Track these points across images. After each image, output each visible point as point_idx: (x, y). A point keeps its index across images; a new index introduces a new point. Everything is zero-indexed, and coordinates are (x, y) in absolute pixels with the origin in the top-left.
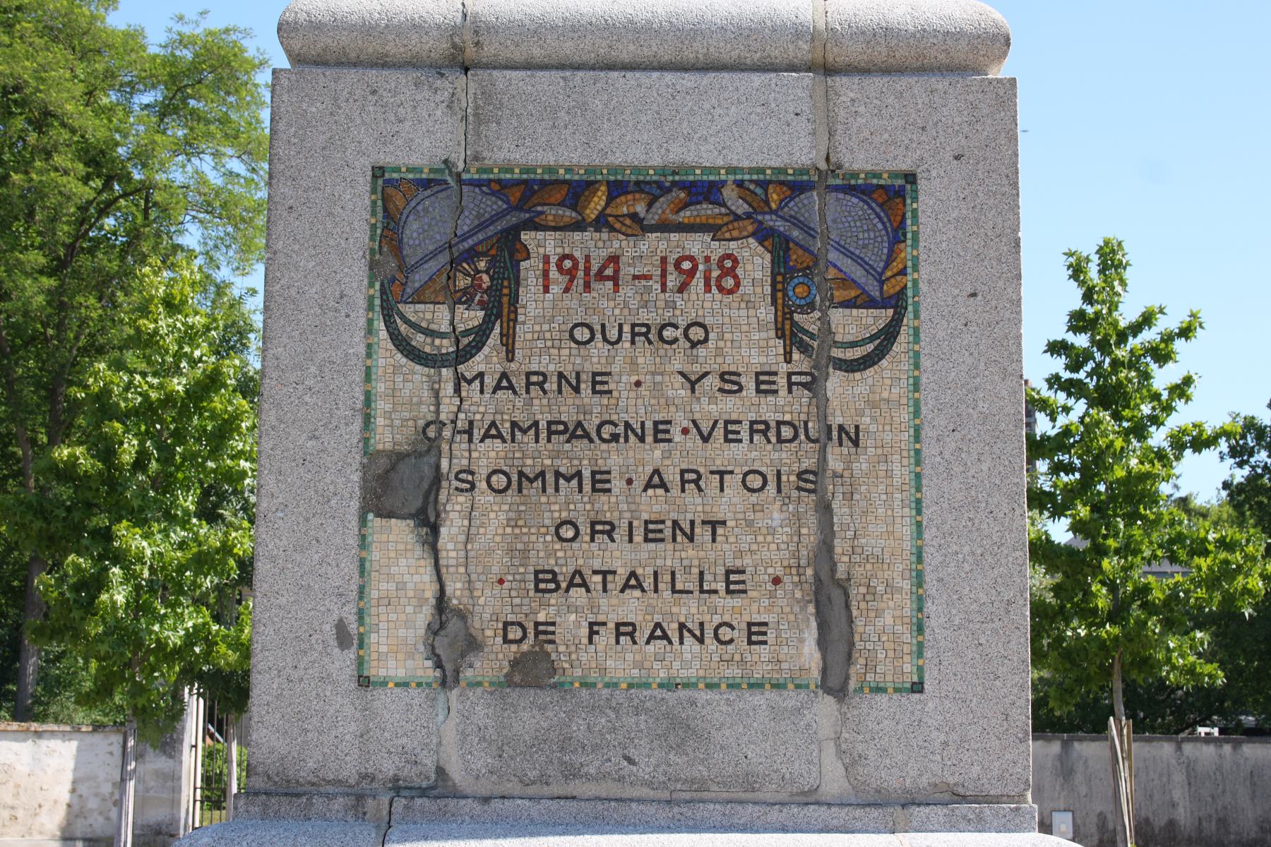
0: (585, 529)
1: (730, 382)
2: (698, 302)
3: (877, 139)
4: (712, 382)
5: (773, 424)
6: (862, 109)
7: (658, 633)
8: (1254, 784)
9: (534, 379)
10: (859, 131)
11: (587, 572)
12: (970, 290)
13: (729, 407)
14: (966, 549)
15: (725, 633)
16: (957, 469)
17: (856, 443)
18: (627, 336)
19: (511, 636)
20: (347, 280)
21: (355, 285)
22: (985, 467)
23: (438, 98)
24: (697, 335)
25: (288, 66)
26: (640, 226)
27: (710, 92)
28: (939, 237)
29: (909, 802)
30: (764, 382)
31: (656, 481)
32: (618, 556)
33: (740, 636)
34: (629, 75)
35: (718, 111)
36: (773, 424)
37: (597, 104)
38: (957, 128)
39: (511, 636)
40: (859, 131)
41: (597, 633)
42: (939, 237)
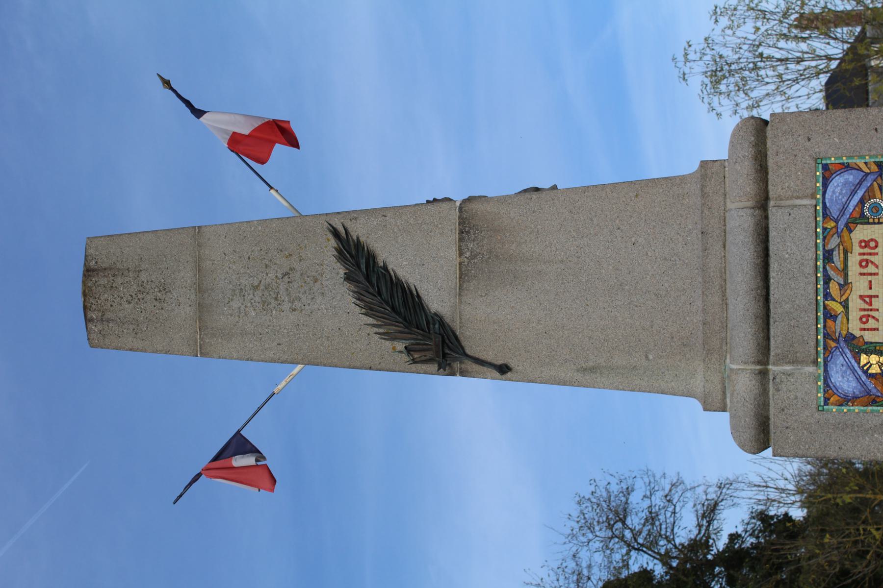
26: (845, 285)
37: (787, 307)
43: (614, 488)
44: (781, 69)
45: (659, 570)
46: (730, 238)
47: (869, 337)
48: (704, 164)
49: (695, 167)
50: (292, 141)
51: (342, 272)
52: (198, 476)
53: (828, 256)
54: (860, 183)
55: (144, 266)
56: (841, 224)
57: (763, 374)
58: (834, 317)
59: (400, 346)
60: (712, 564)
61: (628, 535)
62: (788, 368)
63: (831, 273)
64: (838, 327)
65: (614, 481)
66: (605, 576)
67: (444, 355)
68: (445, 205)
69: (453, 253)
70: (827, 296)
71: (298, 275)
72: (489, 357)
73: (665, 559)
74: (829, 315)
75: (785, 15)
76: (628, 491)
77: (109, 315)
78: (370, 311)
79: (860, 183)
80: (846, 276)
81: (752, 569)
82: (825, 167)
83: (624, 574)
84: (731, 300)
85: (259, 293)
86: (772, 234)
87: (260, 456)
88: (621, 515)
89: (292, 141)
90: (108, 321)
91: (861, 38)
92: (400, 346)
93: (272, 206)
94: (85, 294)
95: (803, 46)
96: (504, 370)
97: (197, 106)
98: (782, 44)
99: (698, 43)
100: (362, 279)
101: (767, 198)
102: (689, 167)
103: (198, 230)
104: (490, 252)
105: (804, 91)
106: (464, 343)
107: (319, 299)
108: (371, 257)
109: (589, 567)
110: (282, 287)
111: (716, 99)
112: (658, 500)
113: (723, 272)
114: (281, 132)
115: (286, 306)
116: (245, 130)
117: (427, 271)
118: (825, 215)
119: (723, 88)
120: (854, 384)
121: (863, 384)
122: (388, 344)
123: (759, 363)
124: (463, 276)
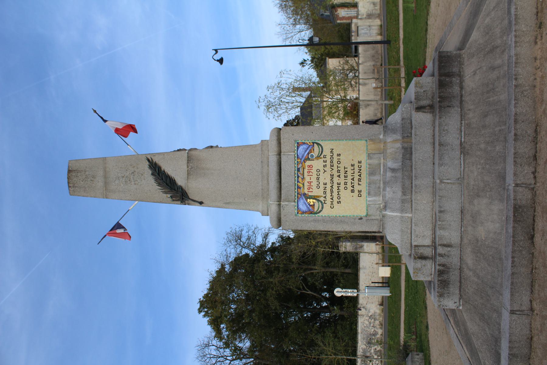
1: (325, 166)
2: (314, 171)
4: (325, 168)
7: (360, 176)
24: (318, 171)
26: (303, 179)
29: (534, 220)
31: (339, 176)
32: (349, 181)
33: (360, 164)
37: (287, 185)
43: (238, 230)
44: (287, 105)
45: (251, 254)
46: (270, 164)
47: (310, 194)
48: (262, 141)
49: (260, 142)
50: (136, 131)
51: (150, 172)
52: (106, 236)
53: (298, 170)
54: (308, 148)
55: (87, 169)
56: (302, 160)
57: (279, 205)
58: (300, 188)
59: (169, 196)
60: (266, 252)
61: (242, 243)
62: (287, 203)
63: (299, 175)
64: (301, 191)
65: (237, 228)
66: (235, 256)
67: (183, 199)
68: (183, 152)
69: (185, 167)
70: (298, 182)
71: (136, 173)
72: (196, 199)
73: (253, 250)
74: (299, 188)
75: (288, 89)
76: (242, 231)
77: (76, 185)
78: (159, 185)
79: (308, 148)
80: (304, 176)
81: (278, 252)
82: (298, 143)
83: (241, 255)
84: (270, 183)
85: (124, 179)
86: (282, 163)
87: (125, 229)
88: (240, 237)
89: (136, 131)
90: (76, 187)
91: (310, 97)
92: (169, 196)
93: (129, 151)
94: (68, 178)
95: (293, 99)
96: (201, 203)
97: (105, 119)
98: (287, 98)
99: (263, 97)
100: (157, 175)
101: (281, 152)
102: (258, 142)
103: (104, 159)
104: (197, 167)
105: (294, 112)
106: (189, 195)
107: (143, 181)
108: (160, 168)
109: (230, 253)
110: (132, 177)
111: (268, 114)
112: (251, 233)
113: (268, 174)
114: (132, 128)
115: (133, 183)
116: (120, 127)
117: (178, 172)
118: (298, 158)
119: (270, 110)
120: (306, 208)
121: (308, 208)
122: (165, 195)
123: (278, 202)
124: (189, 174)
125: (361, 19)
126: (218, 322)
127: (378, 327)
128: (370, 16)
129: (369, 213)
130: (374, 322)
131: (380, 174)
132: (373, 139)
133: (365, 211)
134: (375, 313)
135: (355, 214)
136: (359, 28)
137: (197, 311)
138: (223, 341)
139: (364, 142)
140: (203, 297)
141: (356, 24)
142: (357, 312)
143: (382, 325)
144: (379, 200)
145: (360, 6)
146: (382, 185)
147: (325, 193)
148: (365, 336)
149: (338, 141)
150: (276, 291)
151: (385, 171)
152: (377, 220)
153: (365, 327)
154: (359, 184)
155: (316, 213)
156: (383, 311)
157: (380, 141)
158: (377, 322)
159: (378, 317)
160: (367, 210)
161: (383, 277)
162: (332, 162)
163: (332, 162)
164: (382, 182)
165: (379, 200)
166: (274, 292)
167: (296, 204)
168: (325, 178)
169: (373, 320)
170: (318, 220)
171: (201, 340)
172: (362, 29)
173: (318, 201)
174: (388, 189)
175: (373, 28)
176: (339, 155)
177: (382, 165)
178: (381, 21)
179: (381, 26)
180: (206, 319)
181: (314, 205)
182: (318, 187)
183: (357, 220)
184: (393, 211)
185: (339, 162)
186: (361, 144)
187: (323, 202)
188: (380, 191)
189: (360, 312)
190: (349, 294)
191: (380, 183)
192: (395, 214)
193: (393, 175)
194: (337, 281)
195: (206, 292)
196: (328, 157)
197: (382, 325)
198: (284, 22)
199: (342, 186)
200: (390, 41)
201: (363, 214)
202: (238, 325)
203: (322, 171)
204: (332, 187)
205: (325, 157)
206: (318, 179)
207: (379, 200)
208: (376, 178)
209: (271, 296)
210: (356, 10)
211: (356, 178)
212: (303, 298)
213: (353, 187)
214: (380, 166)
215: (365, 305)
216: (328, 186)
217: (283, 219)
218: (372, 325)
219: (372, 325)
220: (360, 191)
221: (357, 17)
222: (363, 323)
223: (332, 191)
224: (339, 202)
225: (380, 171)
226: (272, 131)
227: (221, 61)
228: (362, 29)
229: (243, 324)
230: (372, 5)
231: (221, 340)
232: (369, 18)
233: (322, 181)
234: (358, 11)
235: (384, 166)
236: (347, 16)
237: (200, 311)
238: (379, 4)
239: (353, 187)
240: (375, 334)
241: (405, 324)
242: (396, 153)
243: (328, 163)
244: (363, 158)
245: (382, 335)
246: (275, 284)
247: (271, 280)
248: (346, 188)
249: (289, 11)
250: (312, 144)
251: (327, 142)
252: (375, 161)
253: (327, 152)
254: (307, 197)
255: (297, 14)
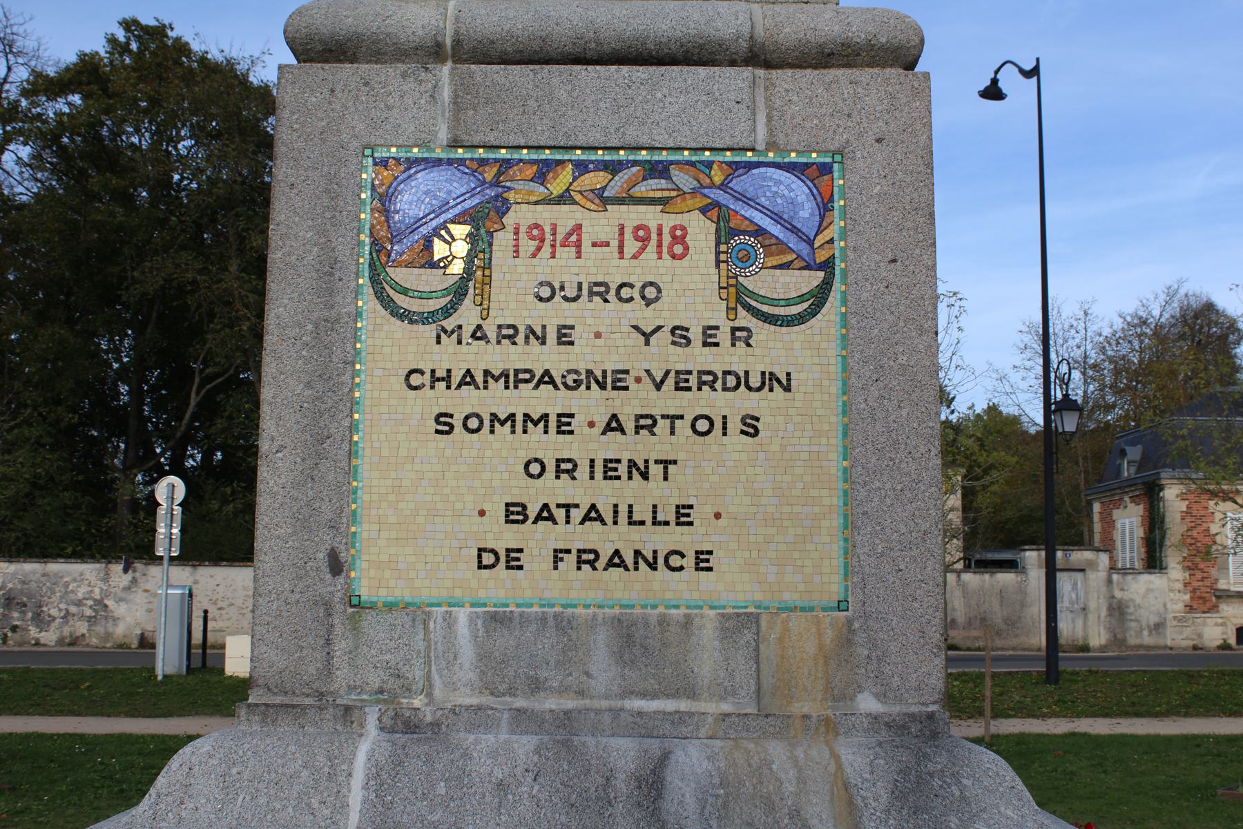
0: (550, 467)
1: (680, 335)
2: (651, 266)
3: (808, 125)
4: (665, 335)
5: (720, 375)
6: (795, 98)
7: (616, 560)
8: (1002, 597)
9: (705, 378)
10: (793, 118)
11: (553, 507)
12: (890, 256)
13: (680, 359)
14: (888, 486)
15: (675, 561)
16: (880, 415)
17: (787, 389)
18: (585, 292)
19: (485, 562)
20: (340, 247)
21: (347, 252)
22: (904, 413)
23: (422, 89)
24: (651, 294)
25: (294, 62)
26: (603, 200)
27: (661, 83)
28: (863, 210)
30: (513, 513)
31: (614, 425)
32: (581, 491)
33: (689, 562)
34: (590, 68)
35: (669, 99)
36: (720, 375)
37: (562, 94)
38: (878, 115)
39: (485, 562)
40: (793, 118)
41: (562, 560)
42: (863, 210)
47: (503, 239)
53: (658, 170)
54: (794, 230)
62: (446, 94)
64: (521, 188)
74: (544, 171)
79: (794, 230)
80: (619, 201)
82: (826, 169)
86: (702, 71)
101: (768, 65)
118: (734, 166)
123: (457, 42)
125: (1109, 581)
126: (89, 83)
127: (66, 631)
128: (1118, 610)
129: (368, 618)
130: (82, 617)
131: (627, 693)
132: (851, 644)
133: (383, 595)
134: (115, 620)
135: (364, 530)
136: (1079, 575)
137: (128, 15)
138: (24, 103)
139: (834, 587)
140: (178, 39)
141: (1093, 565)
142: (117, 559)
143: (71, 644)
144: (458, 686)
145: (1154, 580)
146: (550, 703)
147: (509, 334)
148: (34, 585)
149: (837, 420)
150: (194, 282)
151: (642, 726)
152: (328, 669)
153: (67, 585)
154: (558, 555)
155: (375, 280)
156: (120, 646)
157: (841, 695)
158: (82, 628)
159: (100, 629)
160: (390, 607)
161: (223, 647)
162: (708, 380)
163: (708, 380)
164: (570, 704)
165: (452, 686)
166: (190, 276)
167: (439, 153)
168: (605, 337)
169: (89, 612)
170: (331, 292)
171: (29, 27)
172: (1075, 586)
173: (459, 292)
174: (525, 745)
175: (1080, 623)
176: (751, 427)
177: (684, 705)
178: (1103, 648)
179: (1085, 648)
180: (99, 46)
181: (433, 265)
182: (549, 293)
183: (327, 540)
184: (379, 781)
185: (704, 426)
186: (821, 574)
187: (449, 324)
188: (512, 692)
189: (117, 568)
190: (161, 530)
191: (563, 691)
192: (356, 796)
193: (621, 784)
194: (229, 490)
195: (196, 46)
196: (727, 358)
197: (71, 644)
198: (1093, 328)
199: (549, 446)
200: (1056, 682)
201: (367, 581)
202: (82, 157)
203: (648, 318)
204: (547, 378)
205: (740, 336)
206: (599, 291)
207: (458, 686)
208: (602, 667)
209: (178, 266)
210: (1137, 565)
211: (602, 538)
212: (179, 380)
213: (545, 514)
214: (675, 695)
215: (143, 585)
216: (549, 358)
217: (346, 72)
218: (73, 609)
219: (73, 609)
220: (513, 560)
221: (1113, 568)
222: (81, 577)
223: (514, 379)
224: (444, 424)
225: (643, 695)
226: (901, 18)
227: (993, 92)
228: (1075, 586)
229: (83, 172)
230: (1153, 619)
231: (25, 93)
232: (1110, 609)
233: (587, 316)
234: (1132, 571)
235: (679, 718)
236: (1117, 536)
237: (129, 25)
238: (1161, 642)
239: (545, 514)
240: (40, 620)
241: (27, 737)
242: (770, 805)
243: (698, 358)
244: (731, 585)
245: (37, 644)
246: (220, 281)
247: (233, 268)
248: (534, 468)
249: (1124, 349)
250: (821, 256)
251: (833, 351)
252: (707, 654)
253: (771, 349)
254: (484, 219)
255: (1117, 372)
